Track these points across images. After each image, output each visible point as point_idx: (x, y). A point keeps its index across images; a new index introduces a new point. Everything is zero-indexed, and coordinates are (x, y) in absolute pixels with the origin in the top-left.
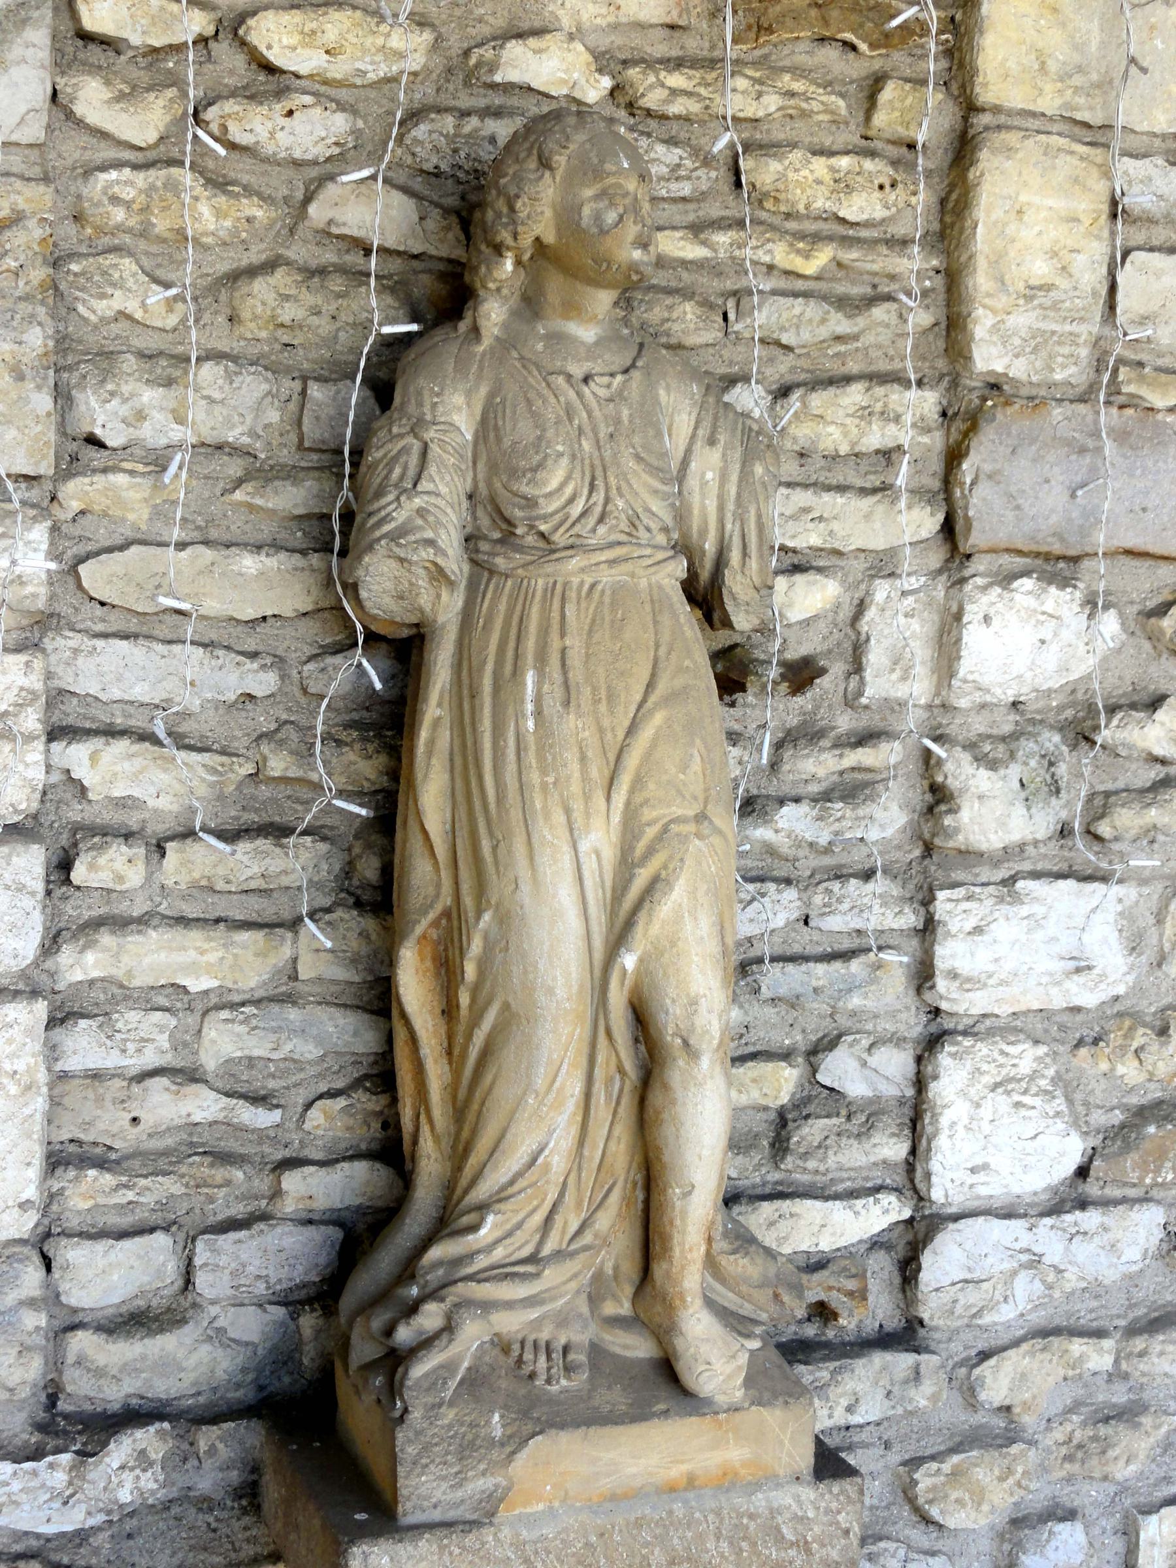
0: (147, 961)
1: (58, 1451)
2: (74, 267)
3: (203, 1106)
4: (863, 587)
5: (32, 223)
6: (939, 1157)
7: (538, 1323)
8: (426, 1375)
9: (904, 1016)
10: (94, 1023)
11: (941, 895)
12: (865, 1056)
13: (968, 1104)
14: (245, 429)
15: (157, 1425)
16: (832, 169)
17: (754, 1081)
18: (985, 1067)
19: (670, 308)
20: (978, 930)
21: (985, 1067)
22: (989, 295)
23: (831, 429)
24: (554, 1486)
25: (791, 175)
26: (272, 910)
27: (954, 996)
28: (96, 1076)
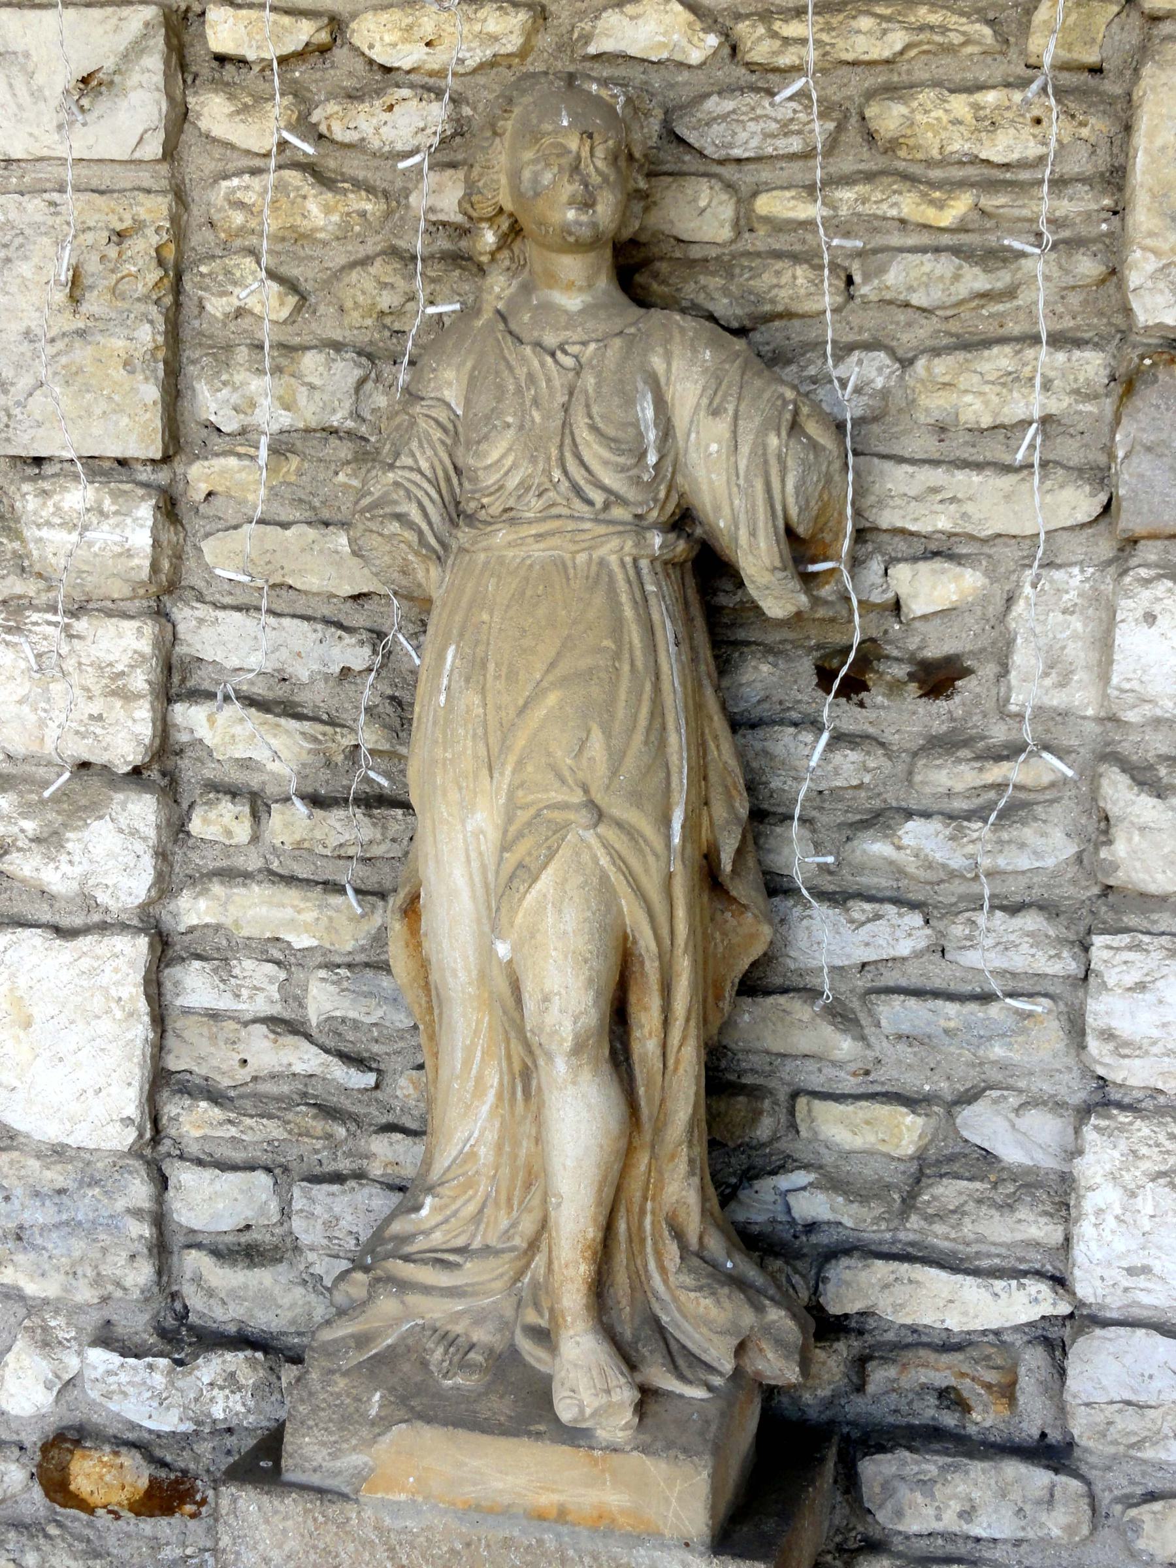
0: (250, 913)
1: (161, 1354)
2: (204, 269)
3: (304, 1059)
4: (1014, 577)
5: (150, 231)
6: (1082, 1246)
7: (457, 1316)
8: (335, 1341)
9: (1066, 1077)
10: (207, 966)
11: (1098, 940)
12: (1012, 1116)
13: (1120, 1191)
14: (346, 413)
15: (249, 1353)
16: (977, 107)
17: (867, 1123)
18: (1144, 1150)
19: (778, 273)
20: (1141, 987)
21: (1144, 1150)
22: (1151, 234)
23: (969, 398)
24: (417, 1480)
25: (920, 118)
26: (375, 879)
27: (1107, 1060)
28: (214, 1016)
